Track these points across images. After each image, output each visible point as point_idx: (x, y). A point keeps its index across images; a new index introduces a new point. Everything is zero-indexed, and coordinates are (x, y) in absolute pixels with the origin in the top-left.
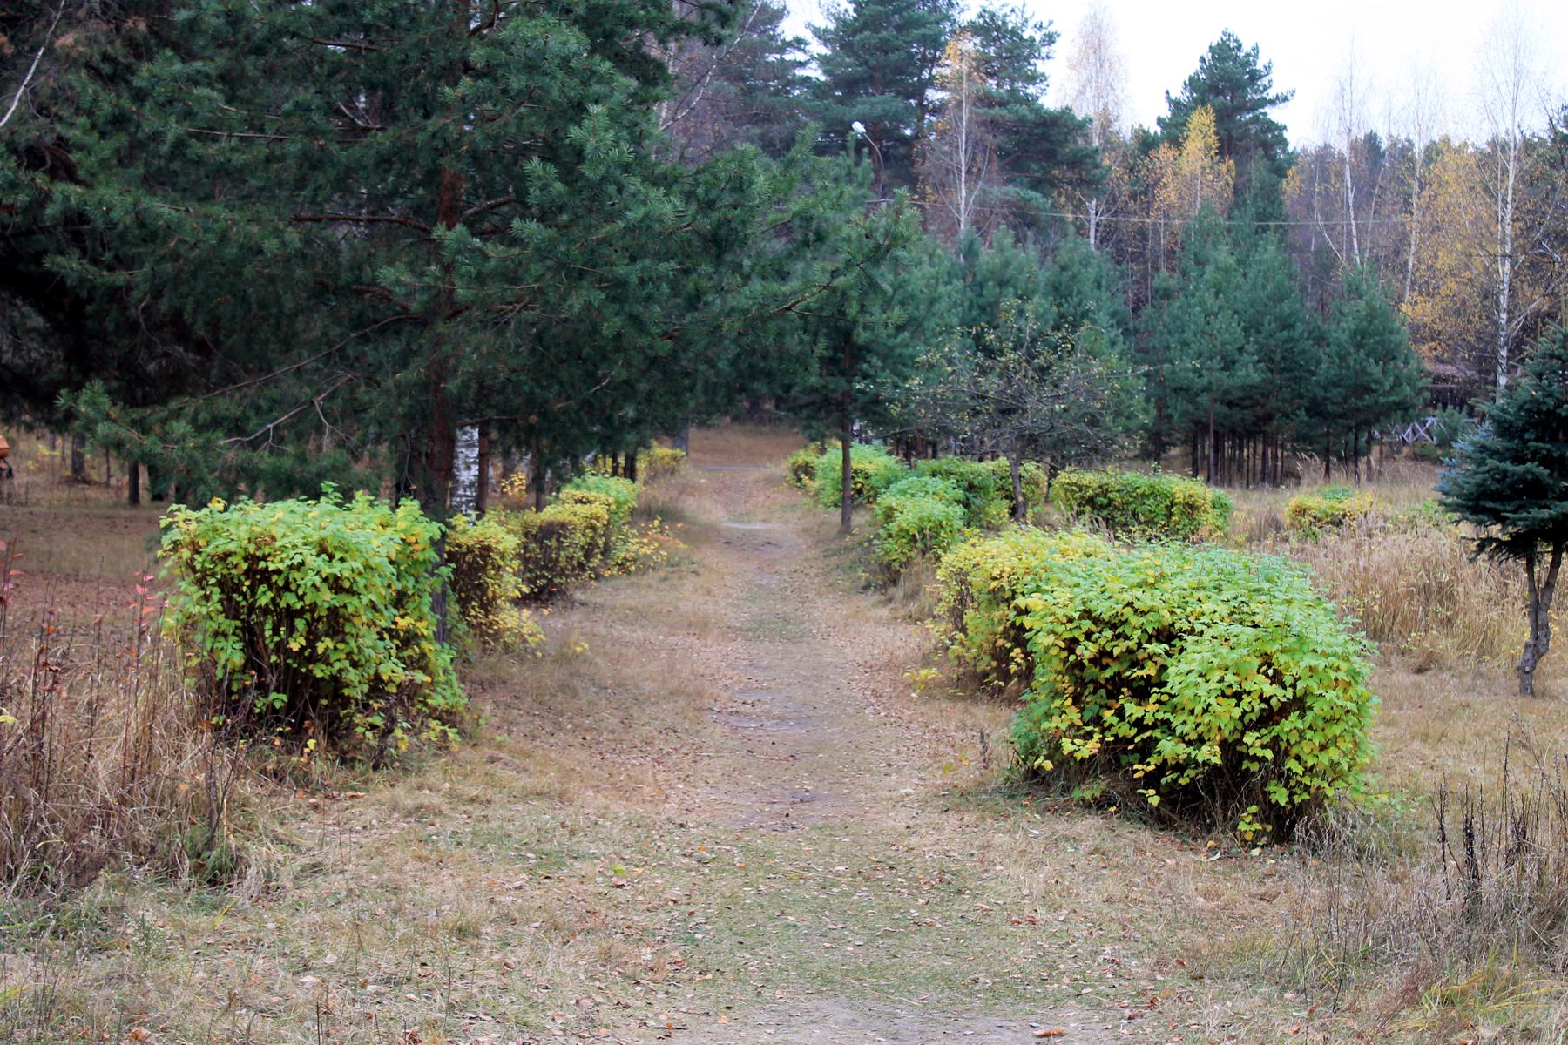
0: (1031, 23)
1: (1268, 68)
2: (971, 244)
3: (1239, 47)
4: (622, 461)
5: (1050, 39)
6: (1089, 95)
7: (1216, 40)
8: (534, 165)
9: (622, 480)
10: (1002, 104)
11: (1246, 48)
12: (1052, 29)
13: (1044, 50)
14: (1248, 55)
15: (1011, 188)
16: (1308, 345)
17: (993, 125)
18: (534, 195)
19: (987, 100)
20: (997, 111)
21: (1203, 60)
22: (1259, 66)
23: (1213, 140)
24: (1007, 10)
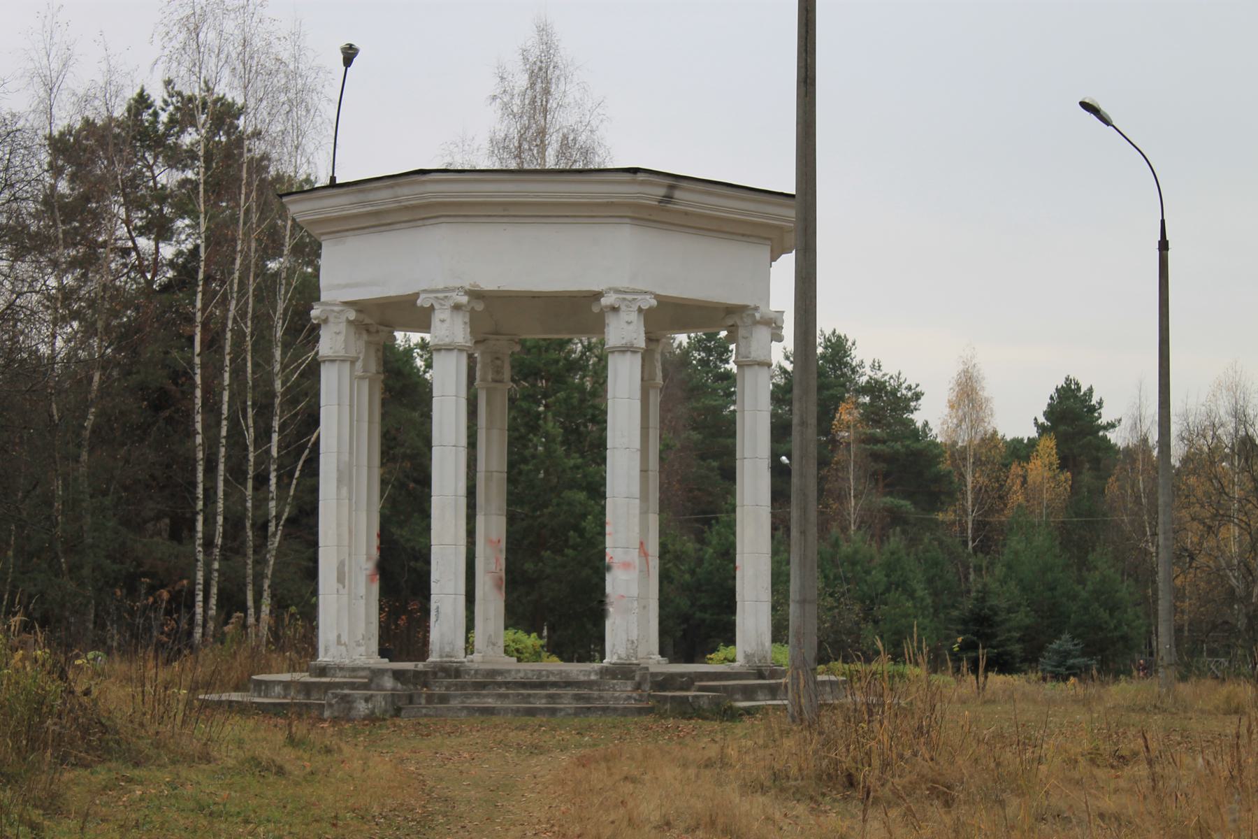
0: (904, 386)
1: (1100, 403)
2: (837, 540)
3: (1079, 389)
4: (146, 116)
5: (917, 396)
6: (964, 427)
7: (1061, 383)
8: (571, 533)
9: (323, 262)
10: (884, 442)
11: (1083, 390)
12: (918, 389)
13: (913, 404)
14: (1085, 394)
15: (888, 499)
16: (1064, 600)
17: (875, 457)
18: (571, 543)
19: (873, 440)
20: (879, 447)
21: (1052, 398)
22: (1093, 402)
23: (1055, 459)
24: (887, 378)
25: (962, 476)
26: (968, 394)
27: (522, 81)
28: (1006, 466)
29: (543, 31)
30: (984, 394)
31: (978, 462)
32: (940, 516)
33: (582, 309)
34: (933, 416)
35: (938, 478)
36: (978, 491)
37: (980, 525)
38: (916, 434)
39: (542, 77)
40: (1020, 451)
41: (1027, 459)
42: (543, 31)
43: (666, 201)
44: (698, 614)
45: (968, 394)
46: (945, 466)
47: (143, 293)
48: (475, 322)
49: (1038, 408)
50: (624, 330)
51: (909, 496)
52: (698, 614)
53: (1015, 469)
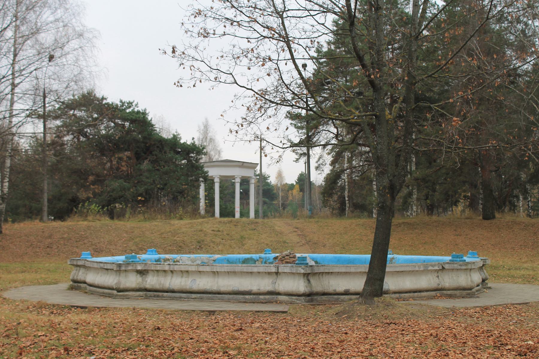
5: (269, 177)
7: (300, 173)
23: (299, 190)
25: (279, 193)
26: (280, 175)
27: (202, 128)
28: (288, 191)
29: (206, 119)
30: (283, 175)
31: (282, 190)
32: (274, 202)
33: (233, 177)
34: (273, 180)
35: (274, 194)
36: (282, 197)
37: (283, 204)
38: (268, 184)
39: (206, 127)
40: (292, 187)
41: (293, 189)
42: (206, 119)
43: (243, 165)
44: (244, 213)
45: (280, 175)
46: (275, 191)
47: (77, 148)
48: (220, 179)
49: (296, 178)
50: (238, 180)
51: (267, 198)
52: (244, 213)
53: (290, 192)
